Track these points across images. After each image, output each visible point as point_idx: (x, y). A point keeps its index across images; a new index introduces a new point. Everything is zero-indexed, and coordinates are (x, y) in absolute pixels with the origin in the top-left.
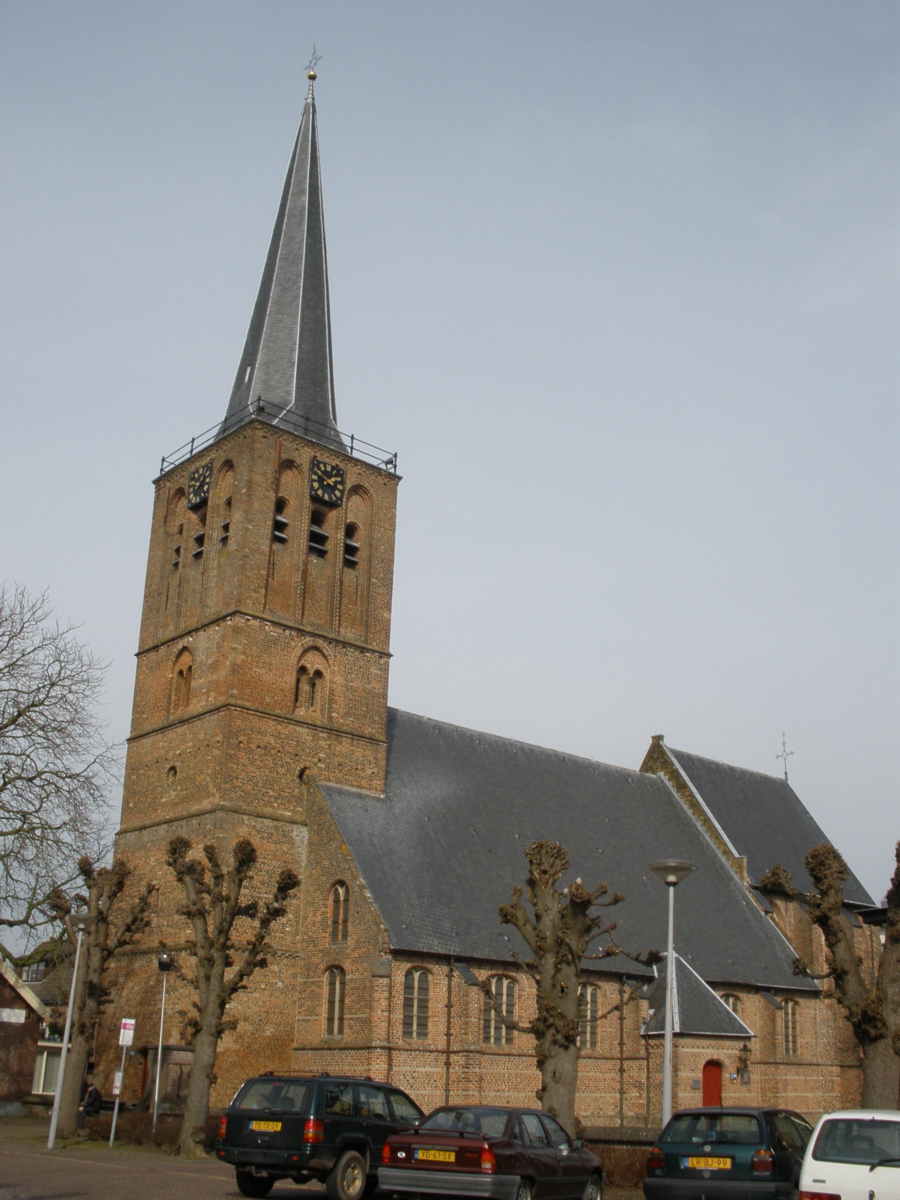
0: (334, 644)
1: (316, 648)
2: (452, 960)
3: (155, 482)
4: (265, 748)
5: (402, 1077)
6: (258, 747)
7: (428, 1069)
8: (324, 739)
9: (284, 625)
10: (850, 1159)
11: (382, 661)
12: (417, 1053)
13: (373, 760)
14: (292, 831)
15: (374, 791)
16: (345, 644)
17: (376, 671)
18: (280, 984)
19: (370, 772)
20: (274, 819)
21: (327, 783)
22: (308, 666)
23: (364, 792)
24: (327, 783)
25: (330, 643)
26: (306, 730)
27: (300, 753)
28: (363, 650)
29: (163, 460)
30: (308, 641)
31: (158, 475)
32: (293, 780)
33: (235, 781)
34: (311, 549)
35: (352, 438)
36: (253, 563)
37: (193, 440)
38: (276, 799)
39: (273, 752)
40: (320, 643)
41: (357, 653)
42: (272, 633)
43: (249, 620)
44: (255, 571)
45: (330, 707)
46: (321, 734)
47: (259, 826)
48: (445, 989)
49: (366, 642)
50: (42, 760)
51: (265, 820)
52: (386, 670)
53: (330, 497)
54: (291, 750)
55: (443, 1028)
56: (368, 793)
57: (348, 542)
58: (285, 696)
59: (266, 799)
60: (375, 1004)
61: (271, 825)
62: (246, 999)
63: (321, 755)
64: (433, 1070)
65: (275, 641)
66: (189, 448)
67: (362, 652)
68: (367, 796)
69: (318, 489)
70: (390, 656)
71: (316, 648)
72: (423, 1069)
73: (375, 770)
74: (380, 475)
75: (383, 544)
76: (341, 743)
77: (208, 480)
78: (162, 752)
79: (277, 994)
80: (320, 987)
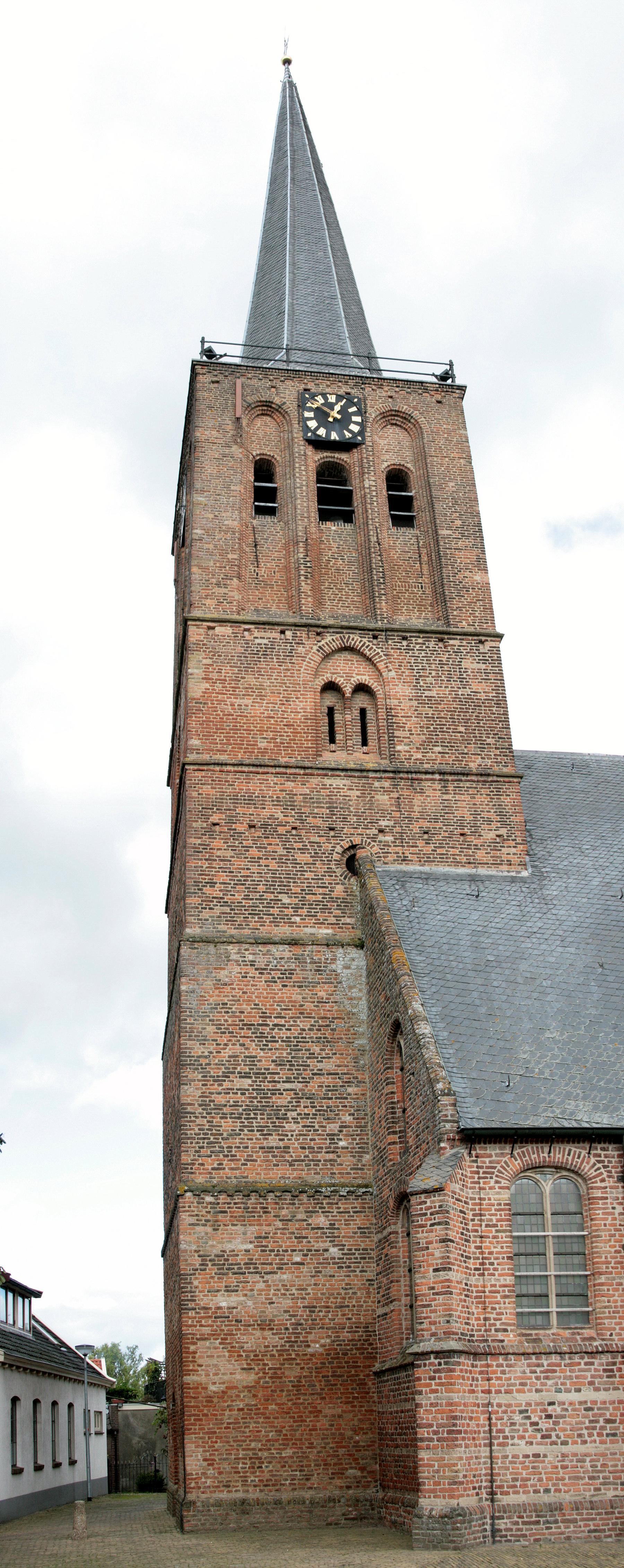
0: (382, 636)
4: (265, 826)
5: (517, 1418)
6: (251, 826)
7: (588, 1395)
8: (386, 791)
10: (527, 1131)
11: (485, 648)
12: (555, 1359)
13: (493, 817)
14: (334, 960)
15: (505, 867)
16: (405, 633)
17: (476, 666)
18: (334, 1251)
19: (492, 835)
20: (293, 943)
21: (404, 867)
22: (340, 680)
23: (482, 871)
24: (404, 867)
26: (347, 782)
27: (339, 825)
28: (442, 636)
30: (330, 640)
32: (330, 872)
33: (207, 890)
36: (211, 546)
39: (281, 830)
40: (355, 639)
41: (432, 644)
42: (257, 641)
43: (210, 628)
44: (218, 557)
46: (377, 784)
47: (261, 961)
49: (448, 624)
51: (273, 948)
52: (495, 660)
53: (341, 434)
54: (319, 822)
56: (492, 872)
58: (295, 733)
59: (275, 911)
61: (287, 954)
62: (262, 1285)
63: (383, 823)
65: (266, 651)
67: (441, 640)
68: (490, 878)
69: (317, 428)
70: (500, 637)
73: (503, 831)
74: (426, 390)
75: (451, 480)
76: (422, 792)
79: (329, 1270)
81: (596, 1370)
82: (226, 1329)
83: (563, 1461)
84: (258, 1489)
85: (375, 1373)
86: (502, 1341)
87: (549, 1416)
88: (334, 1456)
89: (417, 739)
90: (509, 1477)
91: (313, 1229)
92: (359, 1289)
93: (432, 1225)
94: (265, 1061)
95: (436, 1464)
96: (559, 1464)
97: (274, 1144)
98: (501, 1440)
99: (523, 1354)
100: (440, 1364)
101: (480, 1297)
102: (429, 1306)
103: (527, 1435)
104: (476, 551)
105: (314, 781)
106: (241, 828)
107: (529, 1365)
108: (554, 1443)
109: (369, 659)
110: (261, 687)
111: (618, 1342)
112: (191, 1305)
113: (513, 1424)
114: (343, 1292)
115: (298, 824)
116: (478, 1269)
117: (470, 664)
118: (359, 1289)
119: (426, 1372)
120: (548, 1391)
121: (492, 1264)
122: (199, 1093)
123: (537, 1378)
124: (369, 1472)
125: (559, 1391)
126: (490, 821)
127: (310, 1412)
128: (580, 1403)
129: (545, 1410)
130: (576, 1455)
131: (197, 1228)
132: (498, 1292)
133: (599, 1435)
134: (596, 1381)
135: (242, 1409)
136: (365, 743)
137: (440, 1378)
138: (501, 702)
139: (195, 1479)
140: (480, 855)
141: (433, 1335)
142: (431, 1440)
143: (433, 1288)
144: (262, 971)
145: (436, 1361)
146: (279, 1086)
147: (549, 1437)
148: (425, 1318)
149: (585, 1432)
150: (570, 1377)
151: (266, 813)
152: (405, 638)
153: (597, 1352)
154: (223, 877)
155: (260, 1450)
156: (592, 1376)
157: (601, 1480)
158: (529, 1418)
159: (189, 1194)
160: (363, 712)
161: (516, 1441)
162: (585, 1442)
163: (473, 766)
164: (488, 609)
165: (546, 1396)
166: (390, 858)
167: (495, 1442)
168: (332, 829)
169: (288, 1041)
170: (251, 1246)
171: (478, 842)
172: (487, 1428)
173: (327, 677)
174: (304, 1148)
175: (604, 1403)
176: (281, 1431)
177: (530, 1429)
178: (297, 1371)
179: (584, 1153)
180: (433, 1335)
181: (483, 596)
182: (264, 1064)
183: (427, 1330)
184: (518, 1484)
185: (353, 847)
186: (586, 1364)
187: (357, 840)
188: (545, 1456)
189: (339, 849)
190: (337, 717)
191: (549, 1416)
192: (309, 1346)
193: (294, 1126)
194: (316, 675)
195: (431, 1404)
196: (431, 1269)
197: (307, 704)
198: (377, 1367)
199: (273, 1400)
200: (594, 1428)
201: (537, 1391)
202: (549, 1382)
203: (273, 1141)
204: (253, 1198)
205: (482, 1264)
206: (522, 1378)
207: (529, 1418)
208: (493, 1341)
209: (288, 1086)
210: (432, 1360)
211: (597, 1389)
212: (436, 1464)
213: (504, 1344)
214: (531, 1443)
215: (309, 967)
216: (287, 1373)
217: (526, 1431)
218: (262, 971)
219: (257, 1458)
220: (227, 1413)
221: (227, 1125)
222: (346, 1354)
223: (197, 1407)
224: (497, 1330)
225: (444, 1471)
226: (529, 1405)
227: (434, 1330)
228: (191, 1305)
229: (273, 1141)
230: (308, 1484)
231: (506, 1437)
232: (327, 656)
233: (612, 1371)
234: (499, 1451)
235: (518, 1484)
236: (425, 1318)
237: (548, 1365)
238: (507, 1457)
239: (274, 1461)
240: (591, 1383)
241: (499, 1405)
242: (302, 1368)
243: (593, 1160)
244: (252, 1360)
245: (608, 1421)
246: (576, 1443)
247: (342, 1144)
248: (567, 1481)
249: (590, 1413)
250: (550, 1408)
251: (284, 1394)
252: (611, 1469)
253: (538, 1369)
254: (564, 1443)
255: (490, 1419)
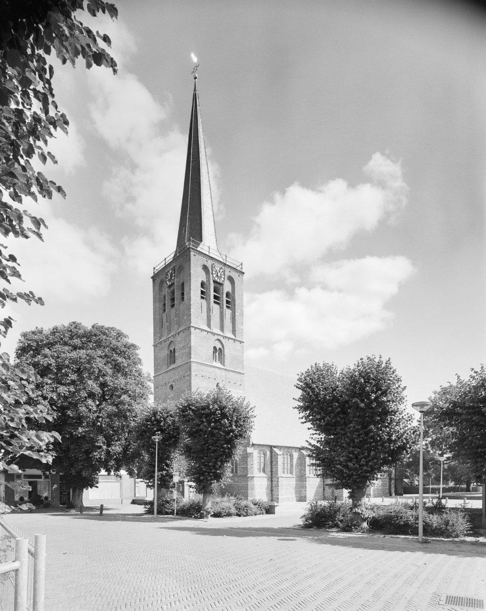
3: (152, 278)
29: (154, 268)
31: (152, 275)
37: (165, 259)
50: (18, 435)
57: (9, 485)
60: (248, 462)
66: (164, 262)
77: (173, 275)
78: (167, 380)
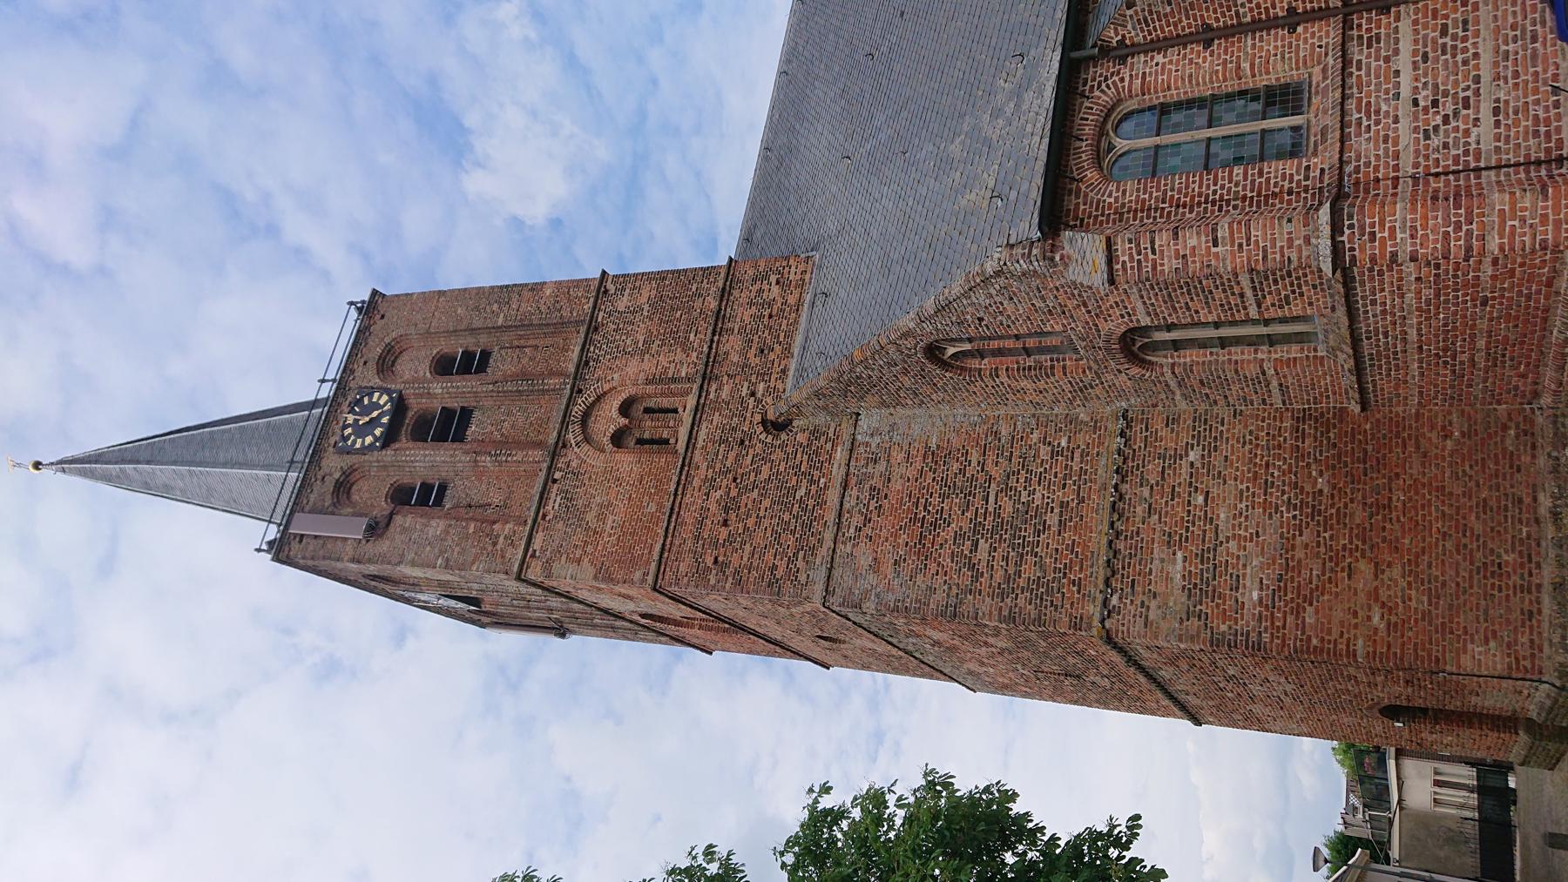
1: (586, 415)
2: (1075, 54)
4: (726, 510)
5: (1436, 141)
6: (725, 523)
7: (1404, 62)
8: (720, 388)
9: (545, 484)
11: (611, 288)
12: (1351, 105)
16: (583, 363)
18: (1192, 456)
19: (775, 289)
22: (612, 429)
24: (791, 373)
25: (580, 391)
26: (704, 426)
27: (739, 435)
28: (593, 327)
32: (782, 446)
33: (779, 573)
34: (460, 437)
35: (323, 381)
38: (812, 482)
39: (734, 493)
45: (674, 380)
48: (1159, 58)
51: (847, 506)
52: (624, 279)
54: (732, 455)
55: (1272, 42)
61: (854, 492)
62: (1232, 544)
63: (745, 391)
64: (1406, 46)
65: (568, 498)
67: (596, 329)
71: (586, 415)
72: (1406, 81)
73: (773, 279)
79: (1217, 461)
80: (1188, 369)
81: (1369, 56)
82: (1290, 596)
83: (1506, 78)
84: (1534, 571)
85: (1363, 409)
86: (1322, 170)
87: (1435, 103)
88: (1483, 466)
89: (680, 356)
90: (1531, 142)
91: (1163, 478)
92: (1246, 426)
93: (1154, 253)
94: (961, 523)
95: (1510, 223)
96: (1511, 82)
97: (1057, 519)
98: (1470, 158)
99: (1342, 142)
100: (1351, 226)
101: (1259, 202)
102: (1265, 251)
103: (1462, 127)
104: (526, 293)
105: (697, 457)
106: (724, 533)
107: (1359, 135)
108: (1477, 93)
109: (599, 399)
110: (601, 505)
111: (1328, 33)
112: (1254, 637)
113: (1446, 145)
114: (1247, 447)
115: (730, 476)
116: (1221, 207)
117: (622, 304)
118: (1246, 426)
119: (1362, 250)
120: (1397, 109)
121: (1215, 192)
122: (988, 600)
123: (1377, 123)
124: (1510, 419)
125: (1397, 96)
126: (761, 291)
127: (1417, 493)
128: (1416, 68)
129: (1426, 110)
130: (1496, 64)
131: (1151, 617)
132: (1253, 181)
133: (1465, 39)
134: (1383, 53)
135: (1409, 583)
136: (675, 411)
137: (1373, 225)
138: (661, 276)
139: (1517, 659)
140: (792, 300)
141: (1307, 240)
142: (1469, 233)
143: (1240, 245)
144: (867, 520)
145: (1347, 232)
146: (991, 509)
147: (1466, 99)
148: (1283, 255)
149: (1459, 58)
150: (1378, 85)
151: (713, 507)
152: (587, 363)
153: (1343, 56)
154: (769, 557)
155: (1472, 563)
156: (1377, 59)
157: (1538, 27)
158: (1436, 128)
159: (1107, 624)
160: (647, 410)
161: (1472, 139)
162: (1476, 55)
163: (714, 305)
164: (577, 283)
165: (1404, 108)
166: (780, 386)
167: (1473, 165)
168: (742, 442)
169: (943, 496)
170: (1179, 555)
171: (780, 300)
172: (1451, 177)
173: (606, 440)
174: (1064, 486)
175: (1416, 42)
176: (1445, 534)
177: (1454, 124)
178: (1356, 508)
179: (1087, 104)
180: (1307, 240)
181: (566, 289)
182: (965, 526)
183: (1300, 251)
184: (1543, 129)
185: (764, 422)
186: (1359, 69)
187: (758, 418)
188: (1497, 100)
189: (763, 437)
190: (647, 436)
191: (1435, 103)
192: (1321, 491)
193: (1038, 495)
194: (603, 451)
195: (1412, 237)
196: (1214, 250)
197: (627, 462)
198: (1355, 408)
199: (1397, 540)
200: (1454, 47)
201: (1396, 121)
202: (1384, 108)
203: (1052, 520)
204: (1120, 545)
205: (1214, 203)
206: (1377, 141)
207: (1436, 128)
208: (1321, 181)
209: (992, 499)
210: (1345, 238)
211: (1396, 52)
212: (1510, 223)
213: (1326, 167)
214: (1477, 120)
215: (870, 469)
216: (1358, 521)
217: (1456, 129)
218: (867, 520)
219: (1486, 569)
220: (1413, 604)
221: (1029, 571)
222: (1335, 445)
223: (1403, 644)
224: (1307, 178)
225: (1523, 209)
226: (1416, 130)
227: (1301, 242)
228: (1254, 637)
229: (1052, 520)
230: (1527, 500)
231: (1466, 153)
232: (587, 439)
233: (1370, 39)
234: (1488, 159)
235: (1543, 129)
236: (1283, 255)
237: (1359, 112)
238: (1498, 149)
239: (1490, 545)
240: (1387, 60)
241: (1416, 165)
242: (1352, 501)
243: (1097, 93)
244: (1337, 565)
245: (1444, 33)
246: (1477, 67)
247: (1064, 443)
248: (1539, 69)
249: (1431, 55)
250: (1422, 103)
251: (1388, 526)
252: (1519, 18)
253: (1365, 123)
254: (1477, 79)
255: (1437, 175)
